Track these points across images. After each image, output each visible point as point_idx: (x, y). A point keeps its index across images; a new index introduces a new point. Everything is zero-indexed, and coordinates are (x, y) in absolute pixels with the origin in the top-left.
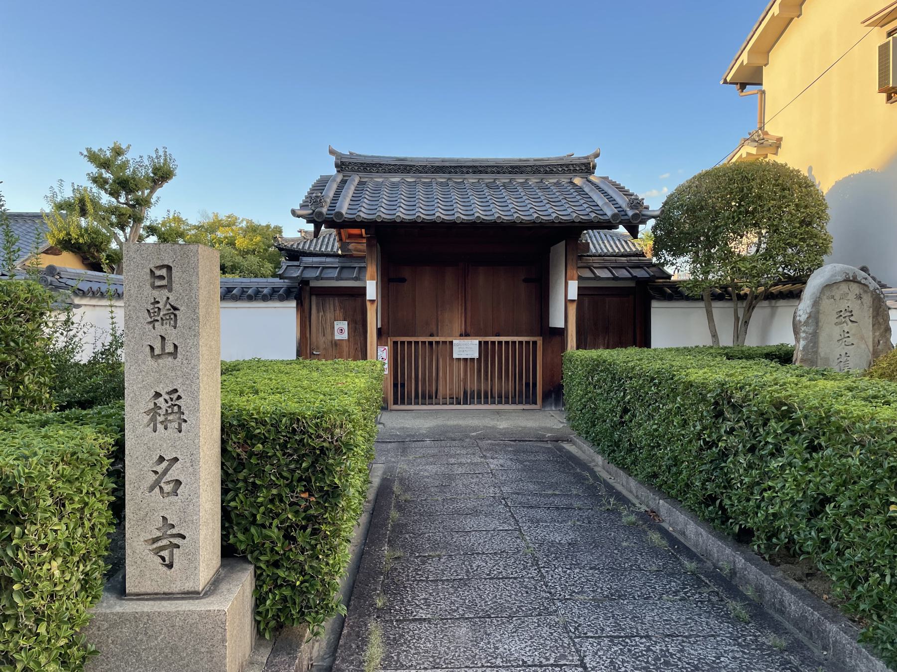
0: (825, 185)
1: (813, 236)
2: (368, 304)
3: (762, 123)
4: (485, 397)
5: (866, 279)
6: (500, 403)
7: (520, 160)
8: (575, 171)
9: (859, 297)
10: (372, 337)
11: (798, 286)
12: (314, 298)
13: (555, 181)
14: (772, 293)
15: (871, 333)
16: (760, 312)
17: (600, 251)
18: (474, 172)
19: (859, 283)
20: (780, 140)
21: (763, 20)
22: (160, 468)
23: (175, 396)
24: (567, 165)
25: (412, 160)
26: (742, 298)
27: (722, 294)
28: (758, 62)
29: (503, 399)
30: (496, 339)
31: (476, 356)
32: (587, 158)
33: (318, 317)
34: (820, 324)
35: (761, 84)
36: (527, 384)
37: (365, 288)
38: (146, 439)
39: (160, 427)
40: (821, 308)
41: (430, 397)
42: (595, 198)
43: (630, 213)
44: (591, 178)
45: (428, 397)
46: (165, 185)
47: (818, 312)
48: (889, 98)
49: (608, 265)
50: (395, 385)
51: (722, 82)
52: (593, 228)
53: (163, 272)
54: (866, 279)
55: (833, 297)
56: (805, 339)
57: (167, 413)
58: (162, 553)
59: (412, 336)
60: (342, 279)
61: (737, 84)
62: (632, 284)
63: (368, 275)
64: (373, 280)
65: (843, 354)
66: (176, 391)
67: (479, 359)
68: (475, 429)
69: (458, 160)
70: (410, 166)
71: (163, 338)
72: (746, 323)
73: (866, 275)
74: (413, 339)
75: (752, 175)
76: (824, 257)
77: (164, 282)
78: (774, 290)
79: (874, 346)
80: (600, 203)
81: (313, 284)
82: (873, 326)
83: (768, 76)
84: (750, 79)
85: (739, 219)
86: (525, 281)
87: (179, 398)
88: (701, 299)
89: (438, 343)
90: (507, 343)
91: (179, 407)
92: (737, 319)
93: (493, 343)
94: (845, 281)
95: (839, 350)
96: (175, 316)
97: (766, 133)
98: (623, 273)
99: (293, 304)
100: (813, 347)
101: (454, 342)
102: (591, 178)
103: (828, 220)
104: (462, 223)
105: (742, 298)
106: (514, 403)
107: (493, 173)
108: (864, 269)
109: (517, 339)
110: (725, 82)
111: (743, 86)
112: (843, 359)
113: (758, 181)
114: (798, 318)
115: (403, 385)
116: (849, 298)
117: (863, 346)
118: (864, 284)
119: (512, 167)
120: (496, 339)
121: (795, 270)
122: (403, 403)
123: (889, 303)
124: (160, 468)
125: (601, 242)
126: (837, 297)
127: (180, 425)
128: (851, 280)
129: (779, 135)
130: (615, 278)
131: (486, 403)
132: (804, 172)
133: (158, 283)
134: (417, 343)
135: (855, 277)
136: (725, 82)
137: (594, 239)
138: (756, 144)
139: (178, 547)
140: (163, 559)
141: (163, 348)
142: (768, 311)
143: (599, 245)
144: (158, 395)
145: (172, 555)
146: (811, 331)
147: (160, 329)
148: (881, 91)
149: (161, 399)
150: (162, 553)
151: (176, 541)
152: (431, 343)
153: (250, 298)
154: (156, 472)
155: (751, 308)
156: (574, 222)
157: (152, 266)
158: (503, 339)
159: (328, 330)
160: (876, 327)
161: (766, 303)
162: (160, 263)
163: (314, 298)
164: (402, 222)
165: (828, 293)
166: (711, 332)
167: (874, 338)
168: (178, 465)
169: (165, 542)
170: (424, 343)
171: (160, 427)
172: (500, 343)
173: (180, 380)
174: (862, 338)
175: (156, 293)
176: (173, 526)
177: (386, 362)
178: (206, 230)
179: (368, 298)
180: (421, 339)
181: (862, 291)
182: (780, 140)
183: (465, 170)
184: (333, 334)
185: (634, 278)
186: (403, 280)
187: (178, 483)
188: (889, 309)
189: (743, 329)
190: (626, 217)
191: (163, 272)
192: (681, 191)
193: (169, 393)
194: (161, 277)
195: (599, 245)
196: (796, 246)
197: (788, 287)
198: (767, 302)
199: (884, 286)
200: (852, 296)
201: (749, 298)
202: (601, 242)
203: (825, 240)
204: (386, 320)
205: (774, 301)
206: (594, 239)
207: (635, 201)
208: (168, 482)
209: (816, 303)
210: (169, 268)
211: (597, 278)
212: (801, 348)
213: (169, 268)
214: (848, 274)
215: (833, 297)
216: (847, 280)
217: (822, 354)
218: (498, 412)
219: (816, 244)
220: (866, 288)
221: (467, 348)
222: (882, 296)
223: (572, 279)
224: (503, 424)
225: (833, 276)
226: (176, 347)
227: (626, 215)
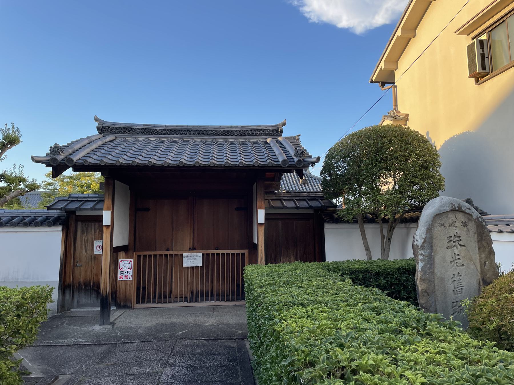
0: (438, 142)
1: (431, 177)
2: (105, 229)
3: (396, 105)
4: (208, 296)
5: (469, 209)
6: (217, 300)
7: (231, 127)
8: (269, 133)
9: (465, 225)
11: (417, 213)
12: (79, 225)
13: (255, 140)
14: (406, 218)
15: (478, 255)
16: (399, 231)
17: (295, 190)
18: (199, 134)
19: (464, 212)
20: (407, 115)
21: (391, 40)
24: (263, 130)
25: (155, 126)
26: (385, 221)
27: (371, 218)
28: (391, 67)
29: (221, 297)
30: (215, 252)
31: (200, 264)
32: (277, 126)
33: (82, 238)
34: (434, 248)
35: (394, 83)
36: (238, 285)
40: (434, 234)
41: (165, 297)
42: (275, 150)
43: (296, 159)
44: (280, 139)
45: (165, 297)
46: (13, 148)
47: (431, 238)
48: (477, 81)
49: (294, 198)
50: (138, 289)
51: (369, 82)
52: (287, 172)
54: (469, 209)
55: (443, 224)
56: (422, 261)
59: (153, 251)
60: (96, 209)
61: (379, 82)
62: (311, 212)
63: (105, 207)
64: (109, 210)
65: (456, 273)
67: (202, 267)
68: (184, 326)
69: (187, 126)
70: (153, 130)
72: (389, 240)
73: (469, 206)
74: (153, 253)
75: (384, 134)
76: (439, 192)
78: (407, 215)
79: (481, 267)
80: (277, 153)
81: (78, 213)
82: (479, 249)
83: (397, 75)
84: (387, 80)
85: (376, 164)
86: (237, 209)
88: (355, 222)
89: (171, 255)
90: (223, 254)
92: (383, 237)
93: (213, 255)
94: (451, 210)
95: (452, 270)
97: (399, 112)
98: (304, 204)
99: (60, 228)
100: (430, 268)
101: (184, 254)
102: (280, 139)
103: (439, 166)
104: (168, 166)
105: (385, 221)
106: (228, 300)
107: (212, 134)
108: (469, 201)
109: (230, 251)
110: (372, 81)
111: (383, 84)
112: (457, 278)
113: (389, 138)
114: (416, 242)
115: (144, 288)
116: (457, 227)
117: (472, 267)
118: (468, 214)
119: (226, 131)
120: (215, 252)
121: (419, 202)
122: (143, 302)
123: (490, 227)
125: (316, 185)
126: (447, 225)
128: (457, 210)
129: (407, 113)
130: (297, 208)
131: (207, 300)
132: (422, 132)
134: (155, 256)
135: (460, 207)
136: (372, 81)
137: (312, 183)
138: (392, 118)
142: (404, 231)
143: (315, 186)
146: (427, 254)
148: (471, 76)
152: (166, 256)
153: (26, 225)
155: (391, 229)
156: (254, 166)
158: (220, 252)
159: (89, 248)
160: (482, 250)
161: (403, 225)
163: (79, 225)
164: (121, 165)
165: (439, 221)
166: (365, 246)
167: (480, 262)
170: (161, 256)
172: (218, 255)
174: (471, 260)
177: (131, 271)
178: (74, 179)
179: (104, 224)
180: (158, 253)
181: (467, 220)
182: (407, 115)
183: (193, 133)
184: (92, 250)
185: (310, 207)
186: (148, 210)
188: (491, 231)
189: (388, 244)
190: (293, 163)
192: (337, 146)
195: (315, 186)
196: (418, 184)
197: (411, 214)
198: (403, 224)
199: (483, 213)
200: (459, 224)
201: (390, 222)
202: (316, 185)
203: (439, 179)
204: (132, 238)
205: (408, 224)
206: (312, 183)
207: (299, 152)
209: (429, 230)
211: (284, 207)
212: (420, 269)
214: (454, 205)
215: (443, 224)
216: (453, 210)
217: (438, 274)
218: (214, 309)
219: (433, 184)
220: (470, 217)
221: (193, 259)
222: (484, 224)
223: (261, 208)
224: (209, 321)
227: (294, 161)
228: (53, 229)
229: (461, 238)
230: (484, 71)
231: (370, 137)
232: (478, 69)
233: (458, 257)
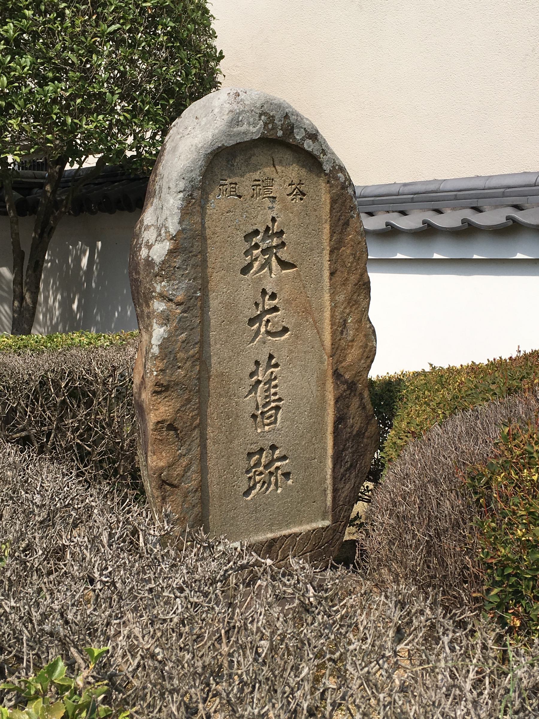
56: (166, 319)
65: (263, 358)
233: (269, 304)
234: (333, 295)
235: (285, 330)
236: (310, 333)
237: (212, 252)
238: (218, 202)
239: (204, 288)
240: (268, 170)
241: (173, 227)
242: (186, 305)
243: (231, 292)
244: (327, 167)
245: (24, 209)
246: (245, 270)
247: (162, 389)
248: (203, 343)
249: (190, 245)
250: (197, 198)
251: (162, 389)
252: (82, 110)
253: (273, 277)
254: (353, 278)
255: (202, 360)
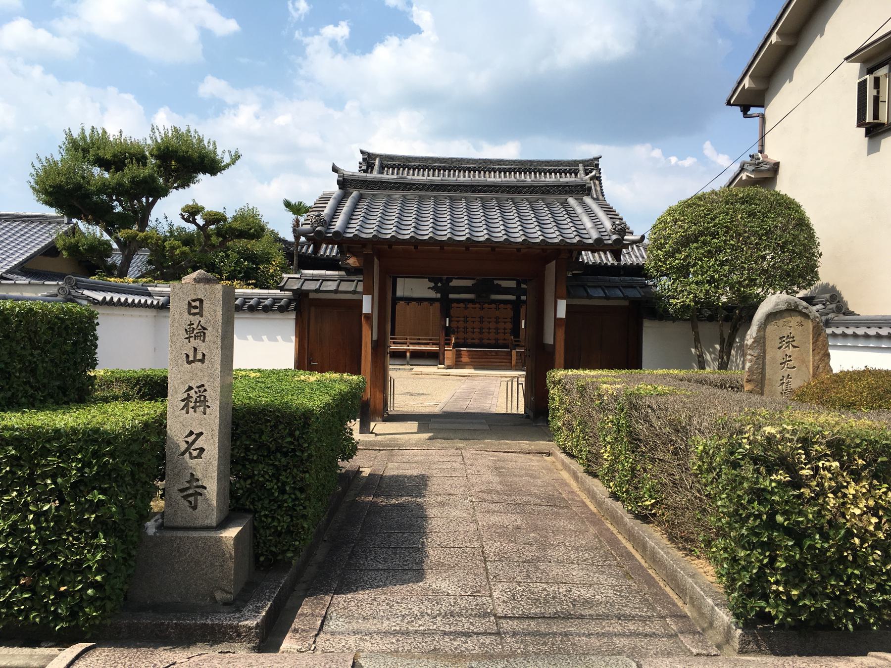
5: (806, 308)
10: (366, 346)
12: (313, 309)
22: (190, 439)
23: (202, 389)
37: (362, 301)
38: (181, 419)
39: (191, 410)
53: (197, 304)
56: (751, 361)
57: (196, 402)
58: (190, 499)
62: (625, 303)
65: (786, 375)
66: (203, 386)
71: (195, 349)
77: (197, 311)
81: (311, 296)
87: (205, 390)
91: (205, 397)
96: (204, 334)
99: (293, 316)
124: (190, 439)
127: (205, 409)
133: (193, 311)
136: (729, 103)
139: (201, 494)
140: (190, 502)
141: (195, 356)
144: (190, 388)
145: (196, 500)
147: (194, 343)
149: (193, 391)
150: (190, 499)
151: (200, 490)
154: (187, 442)
157: (190, 299)
162: (195, 297)
163: (313, 309)
168: (202, 437)
169: (191, 491)
171: (191, 410)
173: (206, 378)
175: (191, 317)
176: (198, 480)
182: (776, 166)
185: (625, 298)
187: (202, 450)
191: (197, 304)
193: (198, 387)
194: (195, 307)
208: (194, 450)
210: (201, 301)
213: (201, 301)
223: (562, 298)
225: (777, 304)
226: (204, 355)
228: (286, 315)
229: (194, 384)
230: (876, 121)
231: (366, 582)
232: (869, 118)
233: (788, 359)
234: (814, 357)
235: (794, 367)
236: (804, 369)
237: (767, 343)
238: (770, 328)
239: (764, 352)
240: (789, 318)
241: (754, 335)
242: (758, 358)
243: (774, 355)
244: (811, 317)
245: (727, 319)
246: (779, 348)
247: (748, 381)
248: (763, 368)
249: (760, 341)
250: (763, 327)
251: (748, 381)
252: (747, 285)
253: (790, 351)
254: (822, 352)
255: (763, 373)
